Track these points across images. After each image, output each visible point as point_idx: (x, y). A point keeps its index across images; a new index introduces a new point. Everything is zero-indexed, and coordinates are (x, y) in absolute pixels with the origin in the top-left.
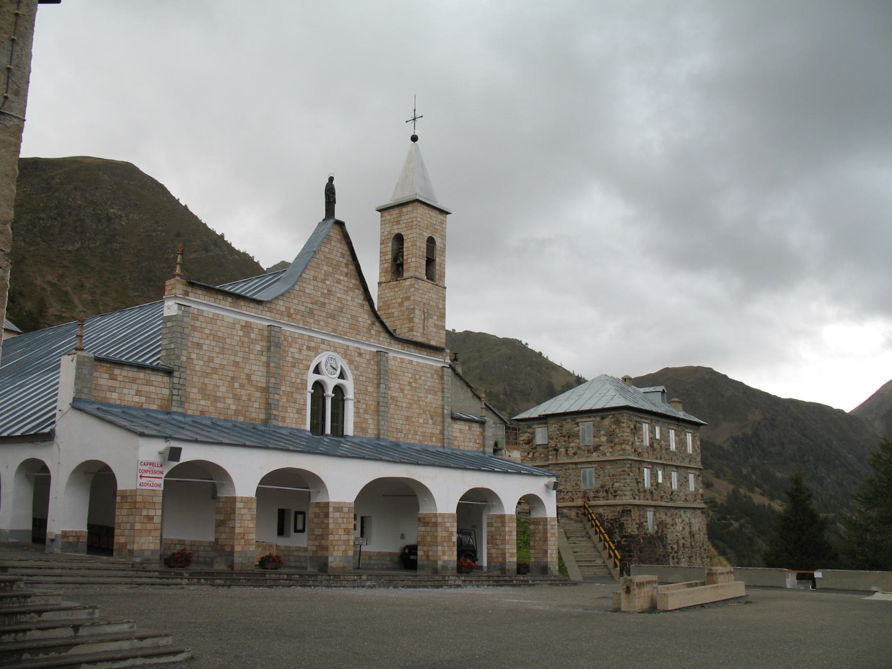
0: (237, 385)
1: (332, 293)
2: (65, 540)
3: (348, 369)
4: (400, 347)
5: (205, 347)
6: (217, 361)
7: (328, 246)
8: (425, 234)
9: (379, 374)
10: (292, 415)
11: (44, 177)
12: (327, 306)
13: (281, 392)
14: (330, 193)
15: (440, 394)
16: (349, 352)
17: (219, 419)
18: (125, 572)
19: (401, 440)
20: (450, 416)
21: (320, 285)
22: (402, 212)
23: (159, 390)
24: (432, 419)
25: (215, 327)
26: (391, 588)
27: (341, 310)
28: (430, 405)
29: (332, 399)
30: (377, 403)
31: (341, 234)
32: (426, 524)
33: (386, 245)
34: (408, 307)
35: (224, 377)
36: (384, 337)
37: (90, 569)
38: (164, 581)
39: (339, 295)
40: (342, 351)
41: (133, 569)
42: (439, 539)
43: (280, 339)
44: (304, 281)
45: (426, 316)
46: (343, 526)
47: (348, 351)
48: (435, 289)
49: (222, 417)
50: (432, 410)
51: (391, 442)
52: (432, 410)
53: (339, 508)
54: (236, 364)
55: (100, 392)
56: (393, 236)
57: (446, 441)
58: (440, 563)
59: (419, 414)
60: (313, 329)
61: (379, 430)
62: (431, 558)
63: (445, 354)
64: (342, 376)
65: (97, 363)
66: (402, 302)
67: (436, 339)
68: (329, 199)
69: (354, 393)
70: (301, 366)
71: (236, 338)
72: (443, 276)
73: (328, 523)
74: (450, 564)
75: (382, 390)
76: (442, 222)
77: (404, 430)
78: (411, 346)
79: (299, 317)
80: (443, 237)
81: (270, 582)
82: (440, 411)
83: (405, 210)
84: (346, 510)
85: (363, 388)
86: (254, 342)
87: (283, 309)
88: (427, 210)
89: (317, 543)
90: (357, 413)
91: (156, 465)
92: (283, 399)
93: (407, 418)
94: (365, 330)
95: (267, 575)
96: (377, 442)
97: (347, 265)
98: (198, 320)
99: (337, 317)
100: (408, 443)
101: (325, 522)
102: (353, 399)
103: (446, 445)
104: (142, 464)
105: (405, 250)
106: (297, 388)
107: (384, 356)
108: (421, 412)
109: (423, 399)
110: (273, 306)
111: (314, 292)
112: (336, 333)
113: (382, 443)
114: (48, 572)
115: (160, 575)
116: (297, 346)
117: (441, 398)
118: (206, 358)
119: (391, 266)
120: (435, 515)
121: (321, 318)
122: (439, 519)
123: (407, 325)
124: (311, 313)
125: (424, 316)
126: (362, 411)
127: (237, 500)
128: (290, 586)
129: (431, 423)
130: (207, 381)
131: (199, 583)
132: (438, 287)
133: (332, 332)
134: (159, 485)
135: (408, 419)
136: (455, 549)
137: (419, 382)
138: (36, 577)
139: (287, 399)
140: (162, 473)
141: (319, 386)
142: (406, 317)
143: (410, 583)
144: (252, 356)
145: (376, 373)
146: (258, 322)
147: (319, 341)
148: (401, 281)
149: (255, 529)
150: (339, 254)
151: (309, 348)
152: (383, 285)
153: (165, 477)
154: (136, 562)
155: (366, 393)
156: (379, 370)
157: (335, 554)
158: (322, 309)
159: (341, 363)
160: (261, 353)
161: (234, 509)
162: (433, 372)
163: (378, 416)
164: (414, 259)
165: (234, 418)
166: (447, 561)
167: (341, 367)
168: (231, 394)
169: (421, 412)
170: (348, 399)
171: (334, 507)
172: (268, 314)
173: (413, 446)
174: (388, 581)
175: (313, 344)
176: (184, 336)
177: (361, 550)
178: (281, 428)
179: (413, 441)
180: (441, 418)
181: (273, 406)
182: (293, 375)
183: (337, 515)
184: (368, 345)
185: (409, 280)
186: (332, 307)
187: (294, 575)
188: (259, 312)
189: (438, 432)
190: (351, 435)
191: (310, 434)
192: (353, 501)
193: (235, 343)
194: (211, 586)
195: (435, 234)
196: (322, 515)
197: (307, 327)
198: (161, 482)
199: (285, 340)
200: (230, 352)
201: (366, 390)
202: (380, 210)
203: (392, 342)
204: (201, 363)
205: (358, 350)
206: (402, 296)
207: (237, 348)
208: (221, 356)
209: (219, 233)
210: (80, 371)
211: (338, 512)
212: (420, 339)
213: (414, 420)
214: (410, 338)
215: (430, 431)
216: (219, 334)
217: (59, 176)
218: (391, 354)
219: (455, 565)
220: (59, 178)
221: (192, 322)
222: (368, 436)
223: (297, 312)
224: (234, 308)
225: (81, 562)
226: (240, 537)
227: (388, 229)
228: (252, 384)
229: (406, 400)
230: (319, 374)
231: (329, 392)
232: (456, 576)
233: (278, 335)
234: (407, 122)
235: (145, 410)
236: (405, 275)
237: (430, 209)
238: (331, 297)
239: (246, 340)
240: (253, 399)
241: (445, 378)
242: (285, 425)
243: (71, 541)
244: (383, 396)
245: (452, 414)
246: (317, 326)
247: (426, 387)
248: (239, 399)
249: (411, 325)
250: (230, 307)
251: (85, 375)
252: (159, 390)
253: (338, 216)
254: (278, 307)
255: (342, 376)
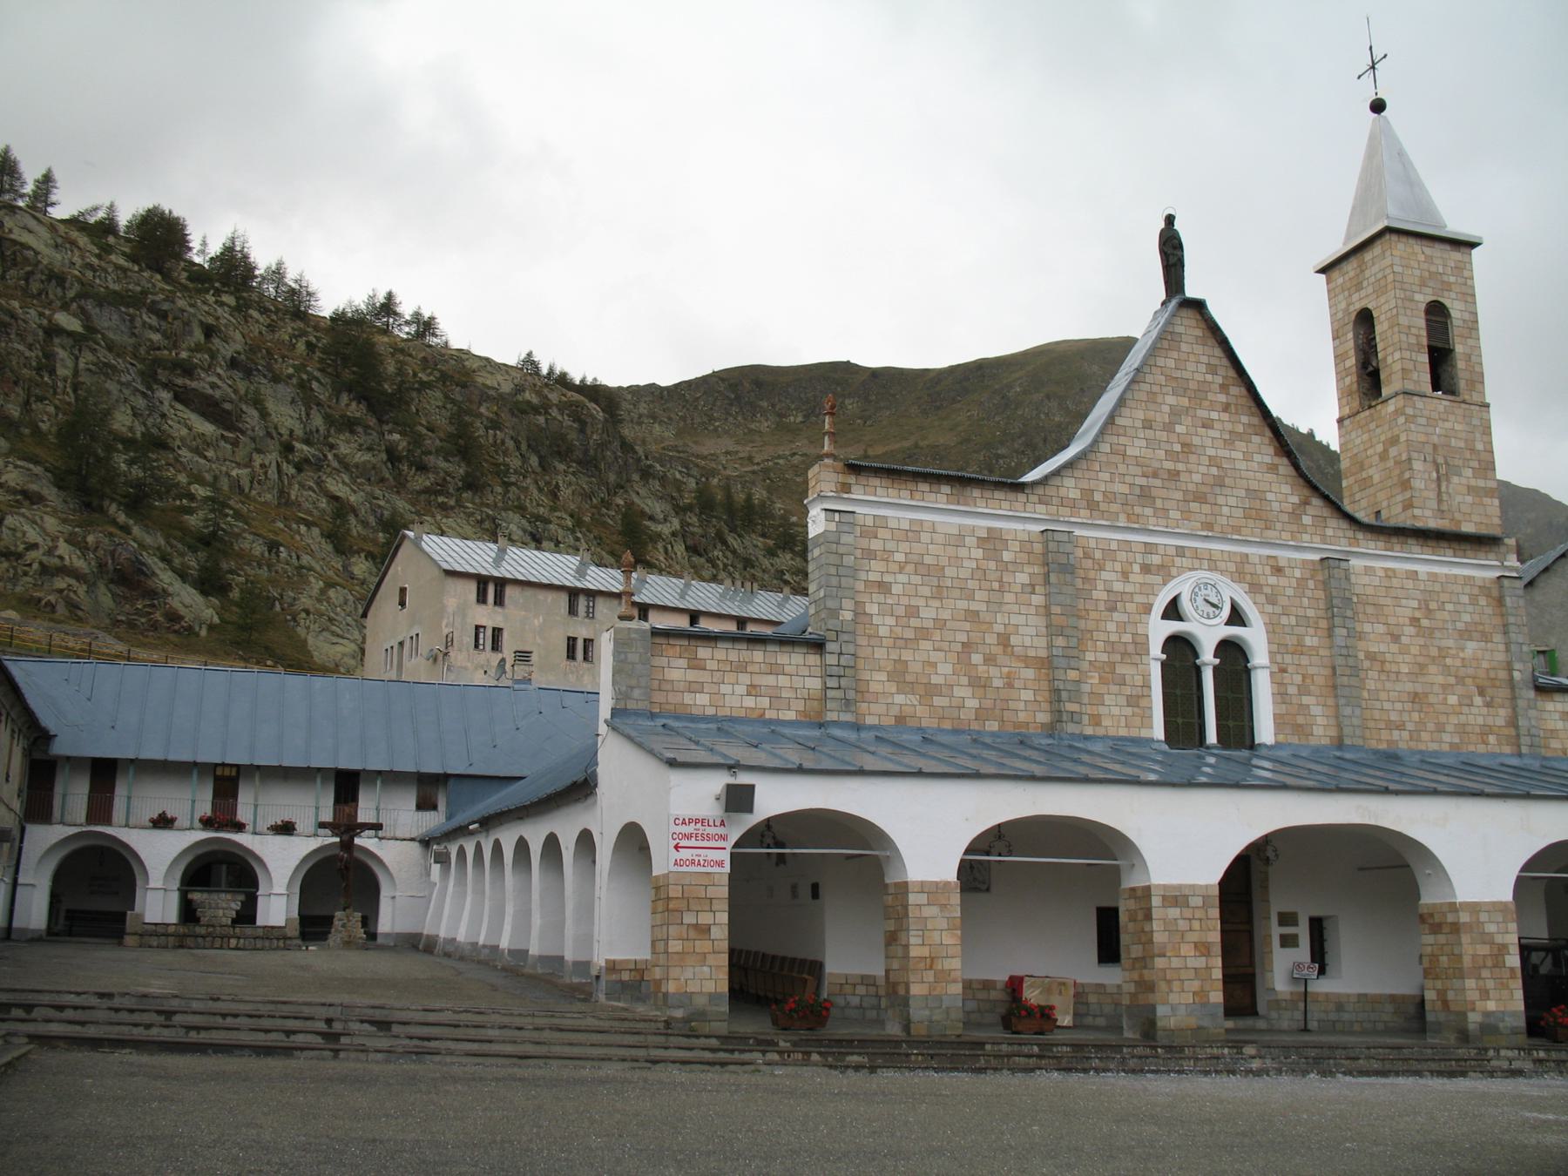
0: (977, 658)
1: (1193, 450)
2: (614, 977)
3: (1251, 603)
4: (1381, 544)
5: (896, 589)
6: (928, 613)
7: (1175, 354)
8: (1418, 297)
9: (1330, 607)
10: (1115, 711)
11: (997, 387)
12: (1183, 477)
13: (1085, 666)
14: (1171, 248)
15: (1498, 638)
16: (1248, 568)
17: (942, 731)
18: (641, 1038)
19: (1402, 745)
20: (1531, 685)
21: (1163, 436)
22: (1364, 263)
23: (797, 682)
24: (1482, 693)
25: (917, 548)
26: (1312, 1075)
27: (1220, 482)
28: (1474, 664)
29: (1216, 669)
30: (1330, 670)
31: (1203, 325)
32: (1436, 929)
33: (1343, 339)
34: (1398, 458)
35: (945, 646)
36: (1335, 526)
37: (561, 1030)
38: (722, 1056)
39: (1211, 452)
40: (1232, 567)
41: (670, 1031)
42: (1467, 962)
43: (1071, 556)
44: (1121, 431)
45: (1443, 471)
46: (1194, 937)
47: (1246, 566)
48: (1459, 412)
49: (947, 725)
50: (1481, 674)
51: (1376, 752)
52: (1481, 674)
53: (1177, 897)
54: (972, 616)
55: (670, 694)
56: (1353, 317)
57: (1525, 740)
58: (1474, 1018)
59: (1444, 687)
60: (1151, 528)
61: (1340, 727)
62: (1453, 1007)
63: (1503, 549)
64: (1236, 617)
65: (658, 640)
66: (1386, 451)
67: (1475, 518)
68: (1168, 261)
69: (1270, 652)
70: (1131, 607)
71: (966, 563)
72: (1477, 380)
73: (1152, 931)
74: (1503, 1021)
75: (1340, 641)
76: (1462, 265)
77: (1407, 724)
78: (1410, 541)
79: (1114, 507)
80: (1469, 296)
81: (986, 1061)
82: (1503, 674)
83: (1368, 256)
84: (1196, 901)
85: (1291, 641)
86: (1010, 567)
87: (1074, 494)
88: (1416, 246)
89: (1135, 976)
90: (1280, 695)
91: (711, 823)
92: (1092, 677)
93: (1414, 698)
94: (1285, 518)
95: (988, 1047)
96: (1338, 754)
97: (1224, 388)
98: (876, 537)
99: (1210, 498)
100: (1421, 752)
101: (1146, 929)
102: (1268, 664)
103: (1524, 750)
104: (677, 822)
105: (1378, 339)
106: (1124, 654)
107: (1339, 568)
108: (1452, 680)
109: (1453, 652)
110: (1050, 491)
111: (1148, 453)
112: (1212, 531)
113: (1348, 756)
114: (472, 1033)
115: (722, 1044)
116: (1118, 567)
117: (1502, 647)
118: (901, 611)
119: (1358, 381)
120: (1454, 908)
121: (1168, 505)
122: (1461, 914)
123: (1399, 498)
124: (1145, 495)
125: (1438, 472)
126: (1292, 690)
127: (910, 888)
128: (1032, 1070)
129: (1481, 704)
130: (907, 655)
131: (807, 1062)
132: (1467, 406)
133: (1202, 530)
134: (720, 864)
135: (1415, 698)
136: (1517, 984)
137: (1439, 615)
138: (437, 1042)
139: (1100, 678)
140: (723, 838)
141: (1180, 647)
142: (1395, 480)
143: (1376, 1065)
144: (1009, 597)
145: (1322, 606)
146: (1019, 526)
147: (1172, 551)
148: (1379, 407)
149: (959, 947)
150: (1203, 368)
151: (1146, 569)
152: (1347, 422)
153: (734, 847)
154: (673, 1018)
155: (1299, 649)
156: (1329, 598)
157: (1174, 998)
158: (1172, 485)
159: (1231, 591)
160: (1029, 589)
161: (905, 907)
162: (1476, 591)
163: (1336, 696)
164: (1397, 355)
165: (975, 726)
166: (1493, 1012)
167: (1231, 599)
168: (966, 678)
169: (1452, 680)
170: (1255, 668)
171: (1164, 897)
172: (1041, 508)
173: (1438, 758)
174: (1311, 1061)
175: (1156, 560)
176: (842, 571)
177: (1309, 989)
178: (1086, 738)
179: (1433, 747)
180: (1509, 690)
181: (1064, 695)
182: (1111, 627)
183: (1174, 912)
184: (1297, 548)
185: (1393, 400)
186: (1197, 478)
187: (1057, 1045)
188: (1019, 506)
189: (1500, 722)
190: (1269, 743)
191: (1165, 747)
192: (1217, 882)
193: (964, 574)
194: (826, 1069)
195: (1446, 294)
196: (1140, 916)
197: (1136, 526)
198: (725, 856)
199: (1087, 556)
200: (957, 593)
201: (1300, 644)
202: (1323, 271)
203: (1360, 535)
204: (890, 621)
205: (1271, 562)
206: (1383, 438)
207: (971, 584)
208: (937, 603)
209: (1304, 430)
210: (622, 656)
211: (1176, 906)
212: (1433, 524)
213: (1432, 699)
214: (1409, 523)
215: (1480, 721)
216: (928, 560)
217: (1019, 382)
218: (1356, 563)
219: (1521, 1023)
220: (1020, 385)
221: (864, 543)
222: (1313, 742)
223: (1110, 497)
224: (958, 504)
225: (552, 1016)
226: (922, 965)
227: (1343, 305)
228: (1013, 653)
229: (1408, 658)
230: (1245, 626)
231: (1208, 657)
232: (1519, 1049)
233: (1068, 548)
234: (1359, 77)
235: (771, 721)
236: (1385, 392)
237: (1425, 242)
238: (1193, 458)
239: (992, 565)
240: (1017, 684)
241: (1508, 601)
242: (1100, 732)
243: (627, 979)
244: (1344, 652)
245: (1535, 679)
246: (1162, 522)
247: (1460, 626)
248: (985, 687)
249: (1408, 494)
250: (948, 502)
251: (633, 663)
252: (797, 682)
253: (1191, 291)
254: (1063, 492)
255: (1236, 617)
